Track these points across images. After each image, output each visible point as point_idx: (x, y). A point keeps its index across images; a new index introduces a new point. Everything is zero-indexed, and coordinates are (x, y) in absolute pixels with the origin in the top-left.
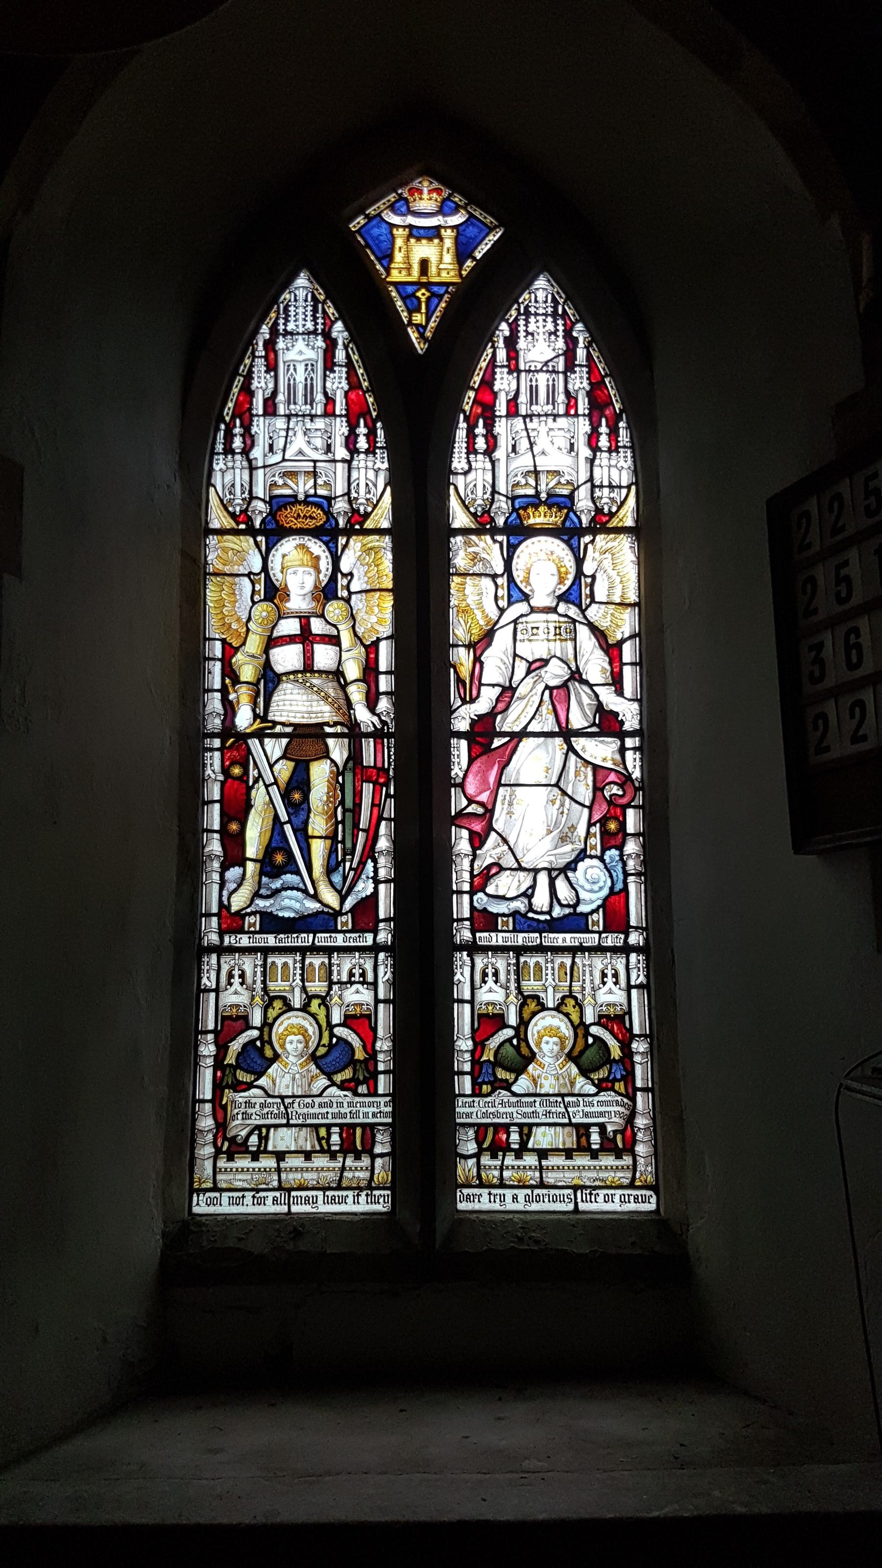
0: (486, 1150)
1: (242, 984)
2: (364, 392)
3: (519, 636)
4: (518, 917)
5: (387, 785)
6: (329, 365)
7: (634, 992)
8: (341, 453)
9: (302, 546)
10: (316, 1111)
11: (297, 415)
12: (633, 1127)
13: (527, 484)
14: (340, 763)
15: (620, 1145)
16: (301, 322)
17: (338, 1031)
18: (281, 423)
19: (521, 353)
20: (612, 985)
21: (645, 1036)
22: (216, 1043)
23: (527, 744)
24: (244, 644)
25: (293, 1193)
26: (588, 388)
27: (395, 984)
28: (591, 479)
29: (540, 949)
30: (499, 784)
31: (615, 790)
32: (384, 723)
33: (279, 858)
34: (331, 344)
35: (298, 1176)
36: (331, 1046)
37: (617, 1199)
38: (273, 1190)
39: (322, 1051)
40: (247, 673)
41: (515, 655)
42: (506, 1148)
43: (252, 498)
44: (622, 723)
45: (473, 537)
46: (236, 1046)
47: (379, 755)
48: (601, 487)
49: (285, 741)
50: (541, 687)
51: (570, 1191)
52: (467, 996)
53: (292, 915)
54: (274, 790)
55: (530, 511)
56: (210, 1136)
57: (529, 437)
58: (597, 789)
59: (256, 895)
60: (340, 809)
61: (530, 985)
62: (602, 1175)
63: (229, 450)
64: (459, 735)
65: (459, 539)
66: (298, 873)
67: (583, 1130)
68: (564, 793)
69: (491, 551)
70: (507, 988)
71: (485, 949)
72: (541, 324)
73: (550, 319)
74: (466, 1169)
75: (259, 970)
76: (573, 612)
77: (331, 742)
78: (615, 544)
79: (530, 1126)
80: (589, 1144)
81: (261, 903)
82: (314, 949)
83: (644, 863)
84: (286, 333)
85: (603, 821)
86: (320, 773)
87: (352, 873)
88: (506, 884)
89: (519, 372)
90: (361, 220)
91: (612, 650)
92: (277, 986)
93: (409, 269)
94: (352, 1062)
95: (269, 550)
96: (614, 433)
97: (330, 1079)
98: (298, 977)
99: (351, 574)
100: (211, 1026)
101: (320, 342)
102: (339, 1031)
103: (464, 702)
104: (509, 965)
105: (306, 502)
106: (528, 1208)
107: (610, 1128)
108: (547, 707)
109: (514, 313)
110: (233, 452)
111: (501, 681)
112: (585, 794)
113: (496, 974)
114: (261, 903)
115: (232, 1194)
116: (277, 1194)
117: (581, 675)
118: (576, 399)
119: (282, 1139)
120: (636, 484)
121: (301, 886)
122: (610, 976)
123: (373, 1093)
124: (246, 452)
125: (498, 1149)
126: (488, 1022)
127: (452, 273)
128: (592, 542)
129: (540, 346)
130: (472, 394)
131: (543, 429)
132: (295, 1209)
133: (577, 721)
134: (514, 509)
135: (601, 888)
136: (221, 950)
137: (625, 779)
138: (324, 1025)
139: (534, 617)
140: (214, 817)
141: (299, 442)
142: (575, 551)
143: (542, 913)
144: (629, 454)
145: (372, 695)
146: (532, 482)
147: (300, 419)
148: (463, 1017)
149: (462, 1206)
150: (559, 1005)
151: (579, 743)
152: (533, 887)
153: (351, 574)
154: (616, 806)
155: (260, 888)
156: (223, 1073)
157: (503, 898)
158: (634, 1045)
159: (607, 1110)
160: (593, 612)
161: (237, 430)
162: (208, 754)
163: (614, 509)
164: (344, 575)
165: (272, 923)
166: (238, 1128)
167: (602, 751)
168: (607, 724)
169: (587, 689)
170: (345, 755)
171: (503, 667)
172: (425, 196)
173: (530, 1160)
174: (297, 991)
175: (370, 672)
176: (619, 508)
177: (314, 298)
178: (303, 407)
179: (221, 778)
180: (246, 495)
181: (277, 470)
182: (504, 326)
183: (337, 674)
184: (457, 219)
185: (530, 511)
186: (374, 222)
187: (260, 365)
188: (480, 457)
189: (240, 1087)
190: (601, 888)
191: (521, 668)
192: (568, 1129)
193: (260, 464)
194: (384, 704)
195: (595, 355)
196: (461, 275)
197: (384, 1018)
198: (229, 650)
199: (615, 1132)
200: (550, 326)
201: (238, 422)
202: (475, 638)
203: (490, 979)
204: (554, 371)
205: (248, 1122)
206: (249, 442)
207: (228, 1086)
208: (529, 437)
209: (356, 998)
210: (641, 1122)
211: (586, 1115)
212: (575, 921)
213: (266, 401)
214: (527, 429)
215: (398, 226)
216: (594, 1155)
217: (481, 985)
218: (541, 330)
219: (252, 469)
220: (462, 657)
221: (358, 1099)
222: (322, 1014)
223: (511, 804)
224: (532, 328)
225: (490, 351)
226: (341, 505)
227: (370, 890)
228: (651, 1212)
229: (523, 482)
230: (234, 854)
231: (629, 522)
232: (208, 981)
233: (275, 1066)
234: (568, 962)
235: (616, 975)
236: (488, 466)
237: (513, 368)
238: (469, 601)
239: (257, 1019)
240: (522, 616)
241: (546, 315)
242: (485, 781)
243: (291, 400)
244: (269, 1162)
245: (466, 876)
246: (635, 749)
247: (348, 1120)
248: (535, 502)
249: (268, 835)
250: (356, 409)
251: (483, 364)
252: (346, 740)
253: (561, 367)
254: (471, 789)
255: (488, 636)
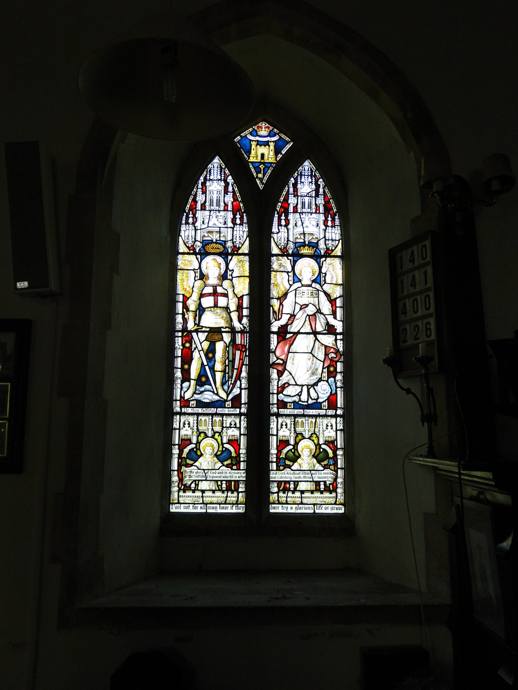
0: (281, 490)
1: (189, 427)
2: (239, 202)
3: (297, 295)
4: (295, 403)
5: (245, 351)
6: (226, 192)
7: (338, 432)
8: (230, 224)
9: (215, 259)
10: (216, 476)
11: (213, 210)
12: (336, 482)
13: (301, 238)
14: (227, 343)
15: (331, 489)
16: (215, 176)
17: (225, 446)
18: (207, 213)
19: (299, 189)
20: (330, 429)
21: (342, 449)
22: (179, 449)
23: (299, 337)
24: (191, 296)
25: (208, 505)
26: (324, 203)
27: (247, 428)
28: (325, 237)
29: (303, 416)
30: (289, 352)
31: (333, 355)
32: (245, 327)
33: (203, 379)
34: (227, 184)
35: (210, 499)
36: (223, 451)
37: (329, 508)
38: (201, 504)
39: (219, 453)
40: (192, 307)
41: (296, 303)
42: (289, 490)
43: (196, 241)
44: (336, 329)
45: (280, 257)
46: (186, 450)
47: (243, 340)
48: (329, 240)
49: (206, 334)
50: (305, 315)
51: (313, 506)
52: (275, 433)
53: (208, 401)
54: (202, 352)
55: (302, 248)
56: (177, 484)
57: (301, 221)
58: (326, 355)
59: (195, 393)
60: (227, 361)
61: (299, 429)
62: (324, 500)
63: (187, 223)
64: (274, 333)
65: (275, 258)
66: (211, 385)
67: (317, 483)
68: (314, 356)
69: (286, 263)
70: (290, 430)
71: (282, 415)
72: (306, 179)
73: (309, 177)
74: (273, 497)
75: (195, 422)
76: (318, 286)
77: (224, 334)
78: (334, 261)
79: (298, 482)
80: (320, 488)
81: (196, 396)
82: (216, 414)
83: (343, 383)
84: (210, 180)
85: (328, 367)
86: (220, 347)
87: (231, 385)
88: (291, 391)
89: (298, 196)
90: (239, 137)
91: (332, 302)
92: (202, 428)
93: (257, 157)
94: (231, 457)
95: (201, 261)
96: (333, 220)
97: (222, 463)
98: (210, 425)
99: (233, 270)
100: (177, 442)
101: (223, 183)
102: (226, 446)
103: (276, 320)
104: (291, 421)
105: (216, 243)
106: (297, 512)
107: (328, 483)
108: (307, 322)
109: (296, 174)
110: (189, 224)
111: (290, 313)
112: (321, 356)
113: (286, 425)
114: (196, 396)
115: (184, 504)
116: (202, 505)
117: (320, 311)
118: (319, 207)
119: (203, 485)
120: (342, 239)
121: (212, 390)
122: (329, 426)
123: (239, 469)
124: (194, 224)
125: (286, 490)
126: (283, 443)
127: (273, 159)
128: (325, 260)
129: (306, 187)
130: (280, 204)
131: (307, 218)
132: (209, 511)
133: (319, 328)
134: (296, 247)
135: (327, 393)
136: (181, 414)
137: (337, 351)
138: (220, 443)
139: (303, 288)
140: (178, 363)
141: (213, 221)
142: (319, 264)
143: (304, 402)
144: (339, 228)
145: (240, 317)
146: (303, 237)
147: (214, 210)
148: (274, 442)
149: (272, 511)
150: (310, 437)
151: (319, 337)
152: (301, 392)
153: (233, 270)
154: (333, 361)
155: (196, 390)
156: (182, 460)
157: (290, 396)
158: (338, 452)
159: (327, 476)
160: (326, 287)
161: (191, 216)
162: (177, 338)
163: (333, 248)
164: (230, 271)
165: (200, 404)
166: (187, 481)
167: (328, 340)
168: (330, 330)
169: (322, 316)
170: (230, 340)
171: (291, 307)
172: (263, 129)
173: (298, 494)
174: (210, 430)
175: (240, 308)
176: (335, 248)
177: (221, 167)
178: (216, 208)
179: (181, 347)
180: (193, 240)
181: (206, 230)
182: (292, 179)
183: (227, 308)
184: (276, 138)
185: (302, 248)
186: (244, 138)
187: (200, 191)
188: (283, 227)
189: (188, 465)
190: (327, 393)
191: (298, 307)
192: (312, 483)
193: (199, 228)
194: (245, 320)
195: (327, 191)
196: (276, 160)
197: (243, 441)
198: (186, 298)
199: (330, 484)
200: (310, 180)
201: (191, 212)
202: (280, 296)
203: (284, 427)
204: (311, 196)
205: (191, 479)
206: (195, 220)
207: (183, 465)
208: (301, 221)
209: (233, 433)
210: (339, 480)
211: (319, 478)
212: (317, 405)
213: (202, 205)
214: (301, 218)
215: (253, 141)
216: (322, 492)
217: (280, 429)
218: (306, 181)
219: (196, 230)
220: (275, 303)
221: (233, 471)
222: (219, 439)
223: (293, 360)
224: (303, 180)
225: (287, 188)
226: (229, 244)
227: (238, 392)
228: (342, 513)
229: (299, 237)
230: (186, 377)
231: (339, 254)
232: (176, 425)
233: (201, 458)
234: (314, 420)
235: (332, 426)
236: (286, 231)
237: (296, 195)
238: (278, 281)
239: (194, 440)
240: (298, 287)
241: (308, 175)
242: (283, 350)
243: (211, 204)
244: (199, 494)
245: (276, 387)
246: (340, 340)
247: (229, 479)
248: (303, 245)
249: (199, 370)
250: (236, 208)
251: (284, 193)
252: (230, 334)
253: (314, 195)
254: (278, 353)
255: (285, 295)
